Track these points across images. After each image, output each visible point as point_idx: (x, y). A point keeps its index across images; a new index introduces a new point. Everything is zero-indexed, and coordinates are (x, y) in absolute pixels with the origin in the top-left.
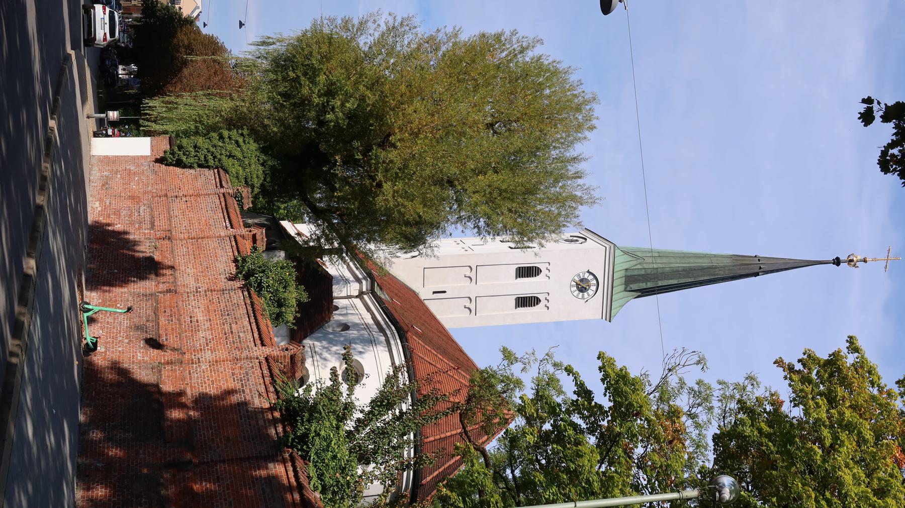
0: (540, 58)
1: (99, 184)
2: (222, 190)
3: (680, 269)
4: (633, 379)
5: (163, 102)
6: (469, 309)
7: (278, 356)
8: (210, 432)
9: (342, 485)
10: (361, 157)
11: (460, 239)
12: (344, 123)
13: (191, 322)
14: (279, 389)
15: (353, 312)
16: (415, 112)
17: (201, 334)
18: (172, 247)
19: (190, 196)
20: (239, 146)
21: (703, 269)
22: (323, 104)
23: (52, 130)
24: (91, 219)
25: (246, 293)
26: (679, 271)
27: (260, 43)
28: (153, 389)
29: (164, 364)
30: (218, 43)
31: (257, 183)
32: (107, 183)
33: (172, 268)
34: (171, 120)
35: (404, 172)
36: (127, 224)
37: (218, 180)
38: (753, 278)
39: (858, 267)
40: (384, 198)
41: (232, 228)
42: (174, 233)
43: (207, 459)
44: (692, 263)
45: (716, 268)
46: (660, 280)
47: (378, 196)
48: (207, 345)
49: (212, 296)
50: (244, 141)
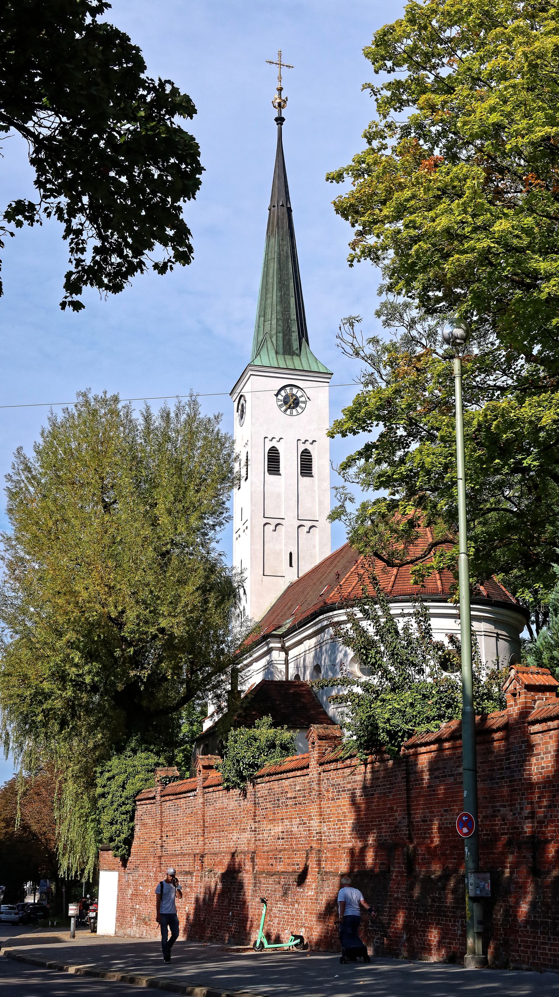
0: (38, 453)
1: (144, 928)
2: (158, 798)
3: (279, 294)
4: (354, 404)
5: (64, 855)
6: (311, 527)
7: (319, 753)
8: (383, 826)
9: (441, 698)
10: (132, 649)
12: (96, 666)
14: (348, 754)
15: (302, 659)
16: (87, 589)
17: (295, 829)
18: (211, 854)
20: (113, 777)
21: (281, 269)
22: (74, 686)
23: (78, 970)
25: (259, 780)
26: (281, 295)
27: (6, 747)
29: (319, 868)
30: (5, 788)
31: (153, 759)
32: (144, 919)
33: (233, 855)
34: (84, 849)
35: (150, 604)
36: (186, 900)
37: (147, 802)
38: (293, 214)
39: (287, 98)
42: (198, 851)
44: (274, 280)
45: (279, 254)
46: (290, 316)
47: (173, 633)
48: (305, 824)
50: (109, 771)
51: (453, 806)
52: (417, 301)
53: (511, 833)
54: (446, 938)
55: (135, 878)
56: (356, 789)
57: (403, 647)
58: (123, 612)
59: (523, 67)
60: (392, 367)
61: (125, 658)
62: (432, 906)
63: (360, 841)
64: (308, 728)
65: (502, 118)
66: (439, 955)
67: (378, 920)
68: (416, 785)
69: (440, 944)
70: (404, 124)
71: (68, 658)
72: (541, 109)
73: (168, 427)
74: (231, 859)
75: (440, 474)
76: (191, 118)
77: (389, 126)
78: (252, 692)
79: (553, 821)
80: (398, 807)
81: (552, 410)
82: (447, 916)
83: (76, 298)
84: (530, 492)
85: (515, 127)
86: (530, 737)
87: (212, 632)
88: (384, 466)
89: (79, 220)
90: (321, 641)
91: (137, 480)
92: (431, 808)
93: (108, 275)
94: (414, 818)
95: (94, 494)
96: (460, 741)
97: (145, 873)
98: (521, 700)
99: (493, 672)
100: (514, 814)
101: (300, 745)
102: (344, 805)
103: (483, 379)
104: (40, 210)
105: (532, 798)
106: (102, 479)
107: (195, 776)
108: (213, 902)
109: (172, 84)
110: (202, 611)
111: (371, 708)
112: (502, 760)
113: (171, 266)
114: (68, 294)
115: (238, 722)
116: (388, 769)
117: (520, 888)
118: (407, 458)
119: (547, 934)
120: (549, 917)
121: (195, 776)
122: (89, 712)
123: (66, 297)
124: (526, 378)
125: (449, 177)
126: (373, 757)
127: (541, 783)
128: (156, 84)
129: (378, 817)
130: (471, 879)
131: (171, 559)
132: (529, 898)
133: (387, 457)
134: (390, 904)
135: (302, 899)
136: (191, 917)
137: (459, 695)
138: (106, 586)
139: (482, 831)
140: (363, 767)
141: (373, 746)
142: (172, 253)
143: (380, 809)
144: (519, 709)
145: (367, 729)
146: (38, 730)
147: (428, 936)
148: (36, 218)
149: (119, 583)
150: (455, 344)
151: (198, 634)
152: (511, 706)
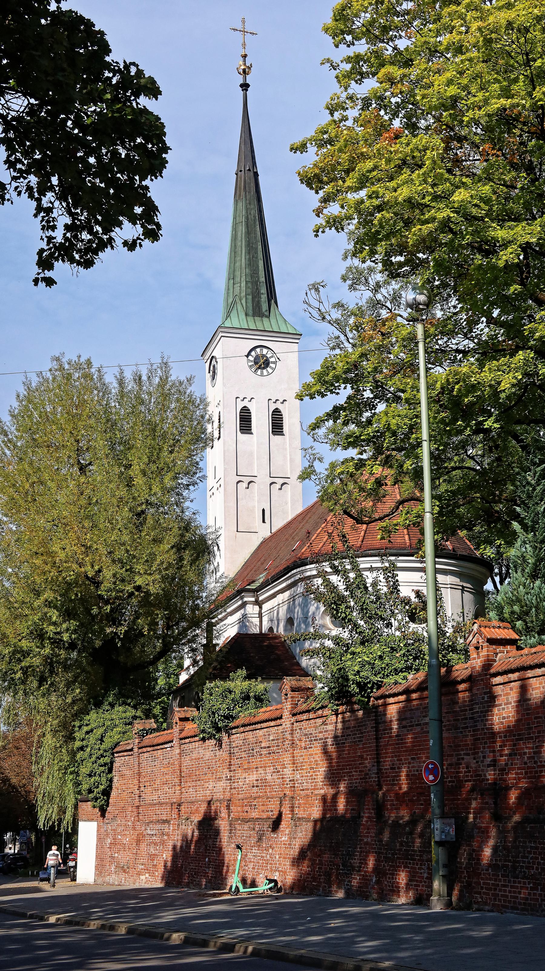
0: (13, 416)
1: (123, 876)
2: (136, 750)
3: (247, 257)
4: (322, 368)
7: (292, 704)
8: (354, 773)
9: (408, 651)
10: (109, 607)
11: (208, 491)
12: (74, 623)
13: (257, 786)
14: (320, 705)
15: (276, 612)
16: (64, 549)
17: (269, 777)
19: (139, 782)
20: (92, 731)
22: (52, 643)
23: (58, 919)
24: (160, 885)
25: (234, 731)
26: (249, 259)
28: (318, 826)
29: (293, 814)
31: (131, 712)
32: (123, 867)
33: (209, 803)
34: (62, 798)
35: (126, 563)
36: (163, 848)
37: (125, 754)
38: (260, 178)
39: (251, 65)
40: (151, 584)
41: (172, 741)
42: (175, 800)
43: (375, 778)
44: (242, 244)
45: (247, 218)
46: (259, 279)
47: (148, 591)
48: (278, 772)
49: (234, 765)
50: (87, 725)
51: (420, 754)
52: (380, 265)
53: (474, 781)
54: (414, 881)
55: (114, 828)
56: (327, 738)
57: (372, 602)
58: (100, 571)
59: (478, 42)
60: (358, 332)
61: (102, 616)
62: (400, 850)
63: (332, 788)
64: (281, 679)
65: (459, 91)
66: (407, 896)
67: (349, 864)
68: (385, 734)
69: (408, 886)
70: (365, 96)
71: (46, 616)
72: (497, 81)
73: (141, 390)
74: (207, 807)
75: (406, 435)
76: (157, 99)
77: (351, 98)
78: (225, 646)
79: (514, 769)
80: (367, 755)
81: (511, 374)
82: (415, 860)
83: (48, 274)
84: (491, 451)
85: (472, 99)
86: (492, 689)
87: (187, 588)
88: (352, 427)
89: (49, 198)
90: (295, 594)
91: (112, 442)
92: (399, 756)
93: (79, 251)
94: (383, 766)
95: (69, 457)
96: (426, 692)
97: (123, 822)
98: (484, 653)
99: (458, 623)
100: (477, 762)
101: (275, 695)
102: (316, 754)
103: (446, 342)
104: (11, 189)
105: (494, 747)
106: (78, 441)
107: (172, 728)
108: (190, 849)
109: (137, 66)
110: (178, 568)
111: (341, 660)
112: (466, 710)
113: (140, 243)
114: (41, 271)
115: (214, 674)
116: (358, 719)
117: (483, 832)
118: (374, 420)
119: (508, 876)
120: (509, 861)
121: (172, 728)
122: (66, 668)
123: (39, 274)
124: (486, 342)
125: (409, 148)
126: (344, 707)
127: (503, 732)
128: (122, 67)
129: (348, 765)
130: (437, 825)
131: (146, 519)
132: (491, 842)
133: (355, 419)
134: (360, 848)
135: (276, 844)
136: (169, 864)
137: (425, 648)
138: (83, 546)
139: (447, 778)
140: (334, 717)
141: (344, 697)
142: (140, 230)
143: (351, 757)
144: (481, 662)
145: (338, 681)
146: (17, 687)
147: (396, 879)
148: (7, 196)
149: (95, 543)
150: (418, 310)
151: (174, 590)
152: (474, 659)
